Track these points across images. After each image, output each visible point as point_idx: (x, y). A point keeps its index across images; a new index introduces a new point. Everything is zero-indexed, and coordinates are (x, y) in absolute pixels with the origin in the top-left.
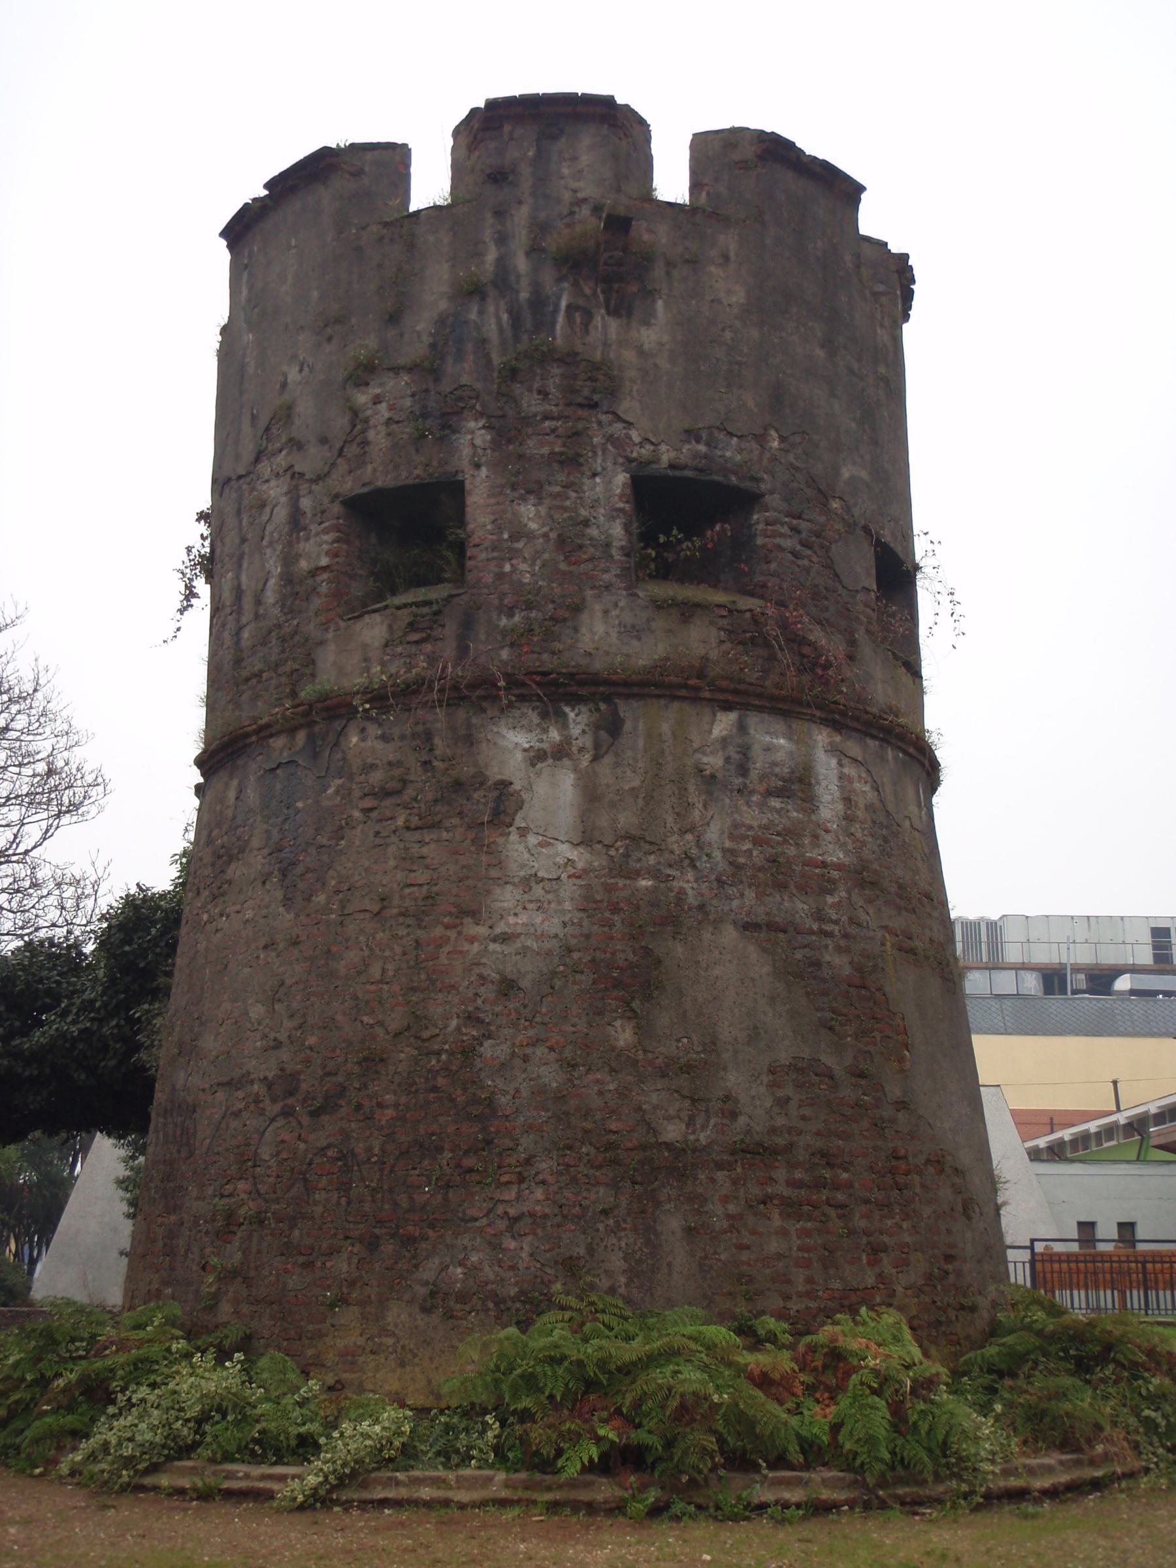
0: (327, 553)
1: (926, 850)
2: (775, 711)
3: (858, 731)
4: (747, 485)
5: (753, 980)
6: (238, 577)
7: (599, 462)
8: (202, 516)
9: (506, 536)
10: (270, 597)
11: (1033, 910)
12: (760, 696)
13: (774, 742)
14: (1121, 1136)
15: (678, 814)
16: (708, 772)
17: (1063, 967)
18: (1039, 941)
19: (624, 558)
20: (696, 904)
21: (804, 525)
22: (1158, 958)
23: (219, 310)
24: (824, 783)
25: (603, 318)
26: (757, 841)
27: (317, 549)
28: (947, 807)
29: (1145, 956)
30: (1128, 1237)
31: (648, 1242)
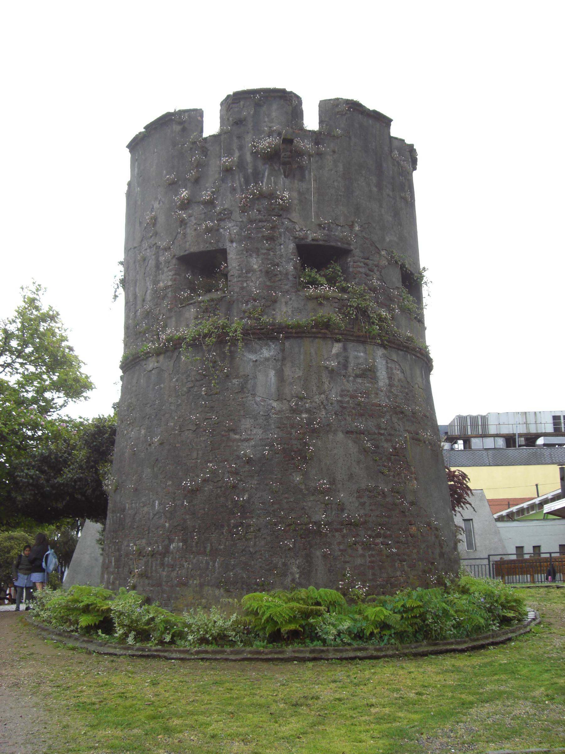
0: (171, 280)
1: (425, 397)
2: (359, 341)
3: (395, 348)
4: (345, 246)
5: (350, 454)
6: (135, 290)
7: (283, 239)
8: (121, 263)
9: (244, 272)
10: (148, 297)
11: (502, 410)
12: (352, 336)
13: (358, 355)
14: (537, 508)
15: (318, 387)
16: (330, 369)
17: (514, 435)
18: (504, 424)
19: (294, 279)
20: (326, 424)
21: (369, 262)
22: (555, 429)
23: (126, 176)
24: (380, 371)
25: (283, 179)
26: (352, 397)
27: (166, 279)
28: (435, 378)
29: (550, 429)
30: (537, 551)
31: (307, 562)
